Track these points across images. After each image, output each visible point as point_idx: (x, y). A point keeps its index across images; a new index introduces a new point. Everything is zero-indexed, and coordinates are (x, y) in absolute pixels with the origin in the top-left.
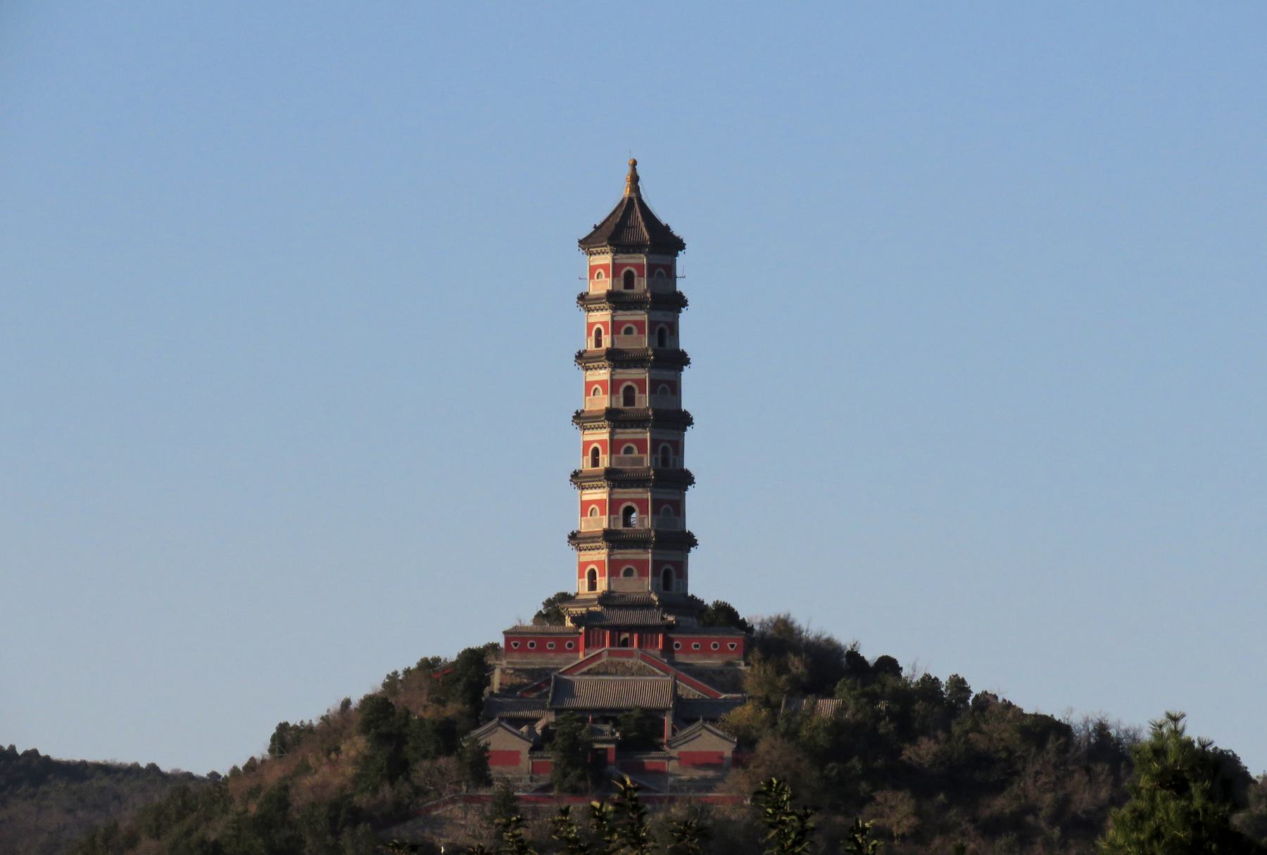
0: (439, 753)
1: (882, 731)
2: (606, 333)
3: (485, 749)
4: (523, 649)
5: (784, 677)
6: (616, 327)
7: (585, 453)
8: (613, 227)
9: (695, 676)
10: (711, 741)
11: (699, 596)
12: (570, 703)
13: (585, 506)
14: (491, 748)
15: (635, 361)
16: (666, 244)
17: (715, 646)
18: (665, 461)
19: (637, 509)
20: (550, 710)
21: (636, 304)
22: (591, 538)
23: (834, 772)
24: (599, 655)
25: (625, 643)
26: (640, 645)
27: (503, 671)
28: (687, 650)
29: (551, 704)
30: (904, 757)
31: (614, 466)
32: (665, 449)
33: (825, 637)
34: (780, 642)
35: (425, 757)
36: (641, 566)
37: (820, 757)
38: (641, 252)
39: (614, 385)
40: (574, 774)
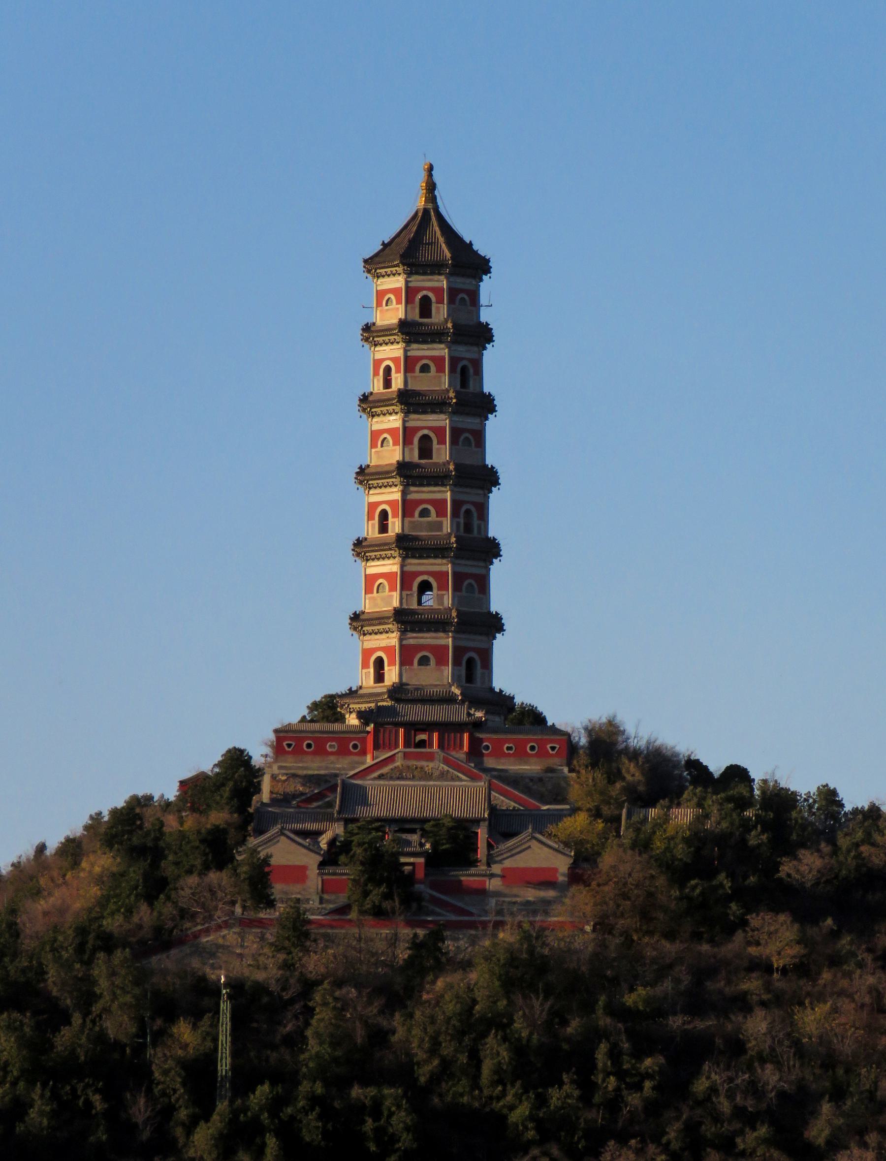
0: (207, 867)
1: (753, 842)
2: (398, 371)
3: (266, 861)
4: (298, 751)
5: (618, 785)
6: (409, 364)
7: (370, 517)
8: (405, 243)
9: (508, 784)
10: (540, 855)
11: (508, 691)
12: (362, 812)
13: (370, 580)
14: (273, 861)
15: (434, 405)
16: (470, 265)
17: (532, 748)
18: (468, 528)
19: (434, 585)
20: (338, 820)
21: (435, 336)
22: (379, 619)
23: (698, 891)
24: (391, 759)
25: (422, 744)
26: (441, 746)
27: (274, 777)
28: (498, 754)
29: (339, 812)
30: (782, 874)
31: (407, 532)
32: (468, 512)
33: (658, 743)
34: (604, 746)
35: (190, 872)
36: (440, 653)
37: (679, 873)
38: (440, 274)
39: (408, 433)
40: (376, 894)
